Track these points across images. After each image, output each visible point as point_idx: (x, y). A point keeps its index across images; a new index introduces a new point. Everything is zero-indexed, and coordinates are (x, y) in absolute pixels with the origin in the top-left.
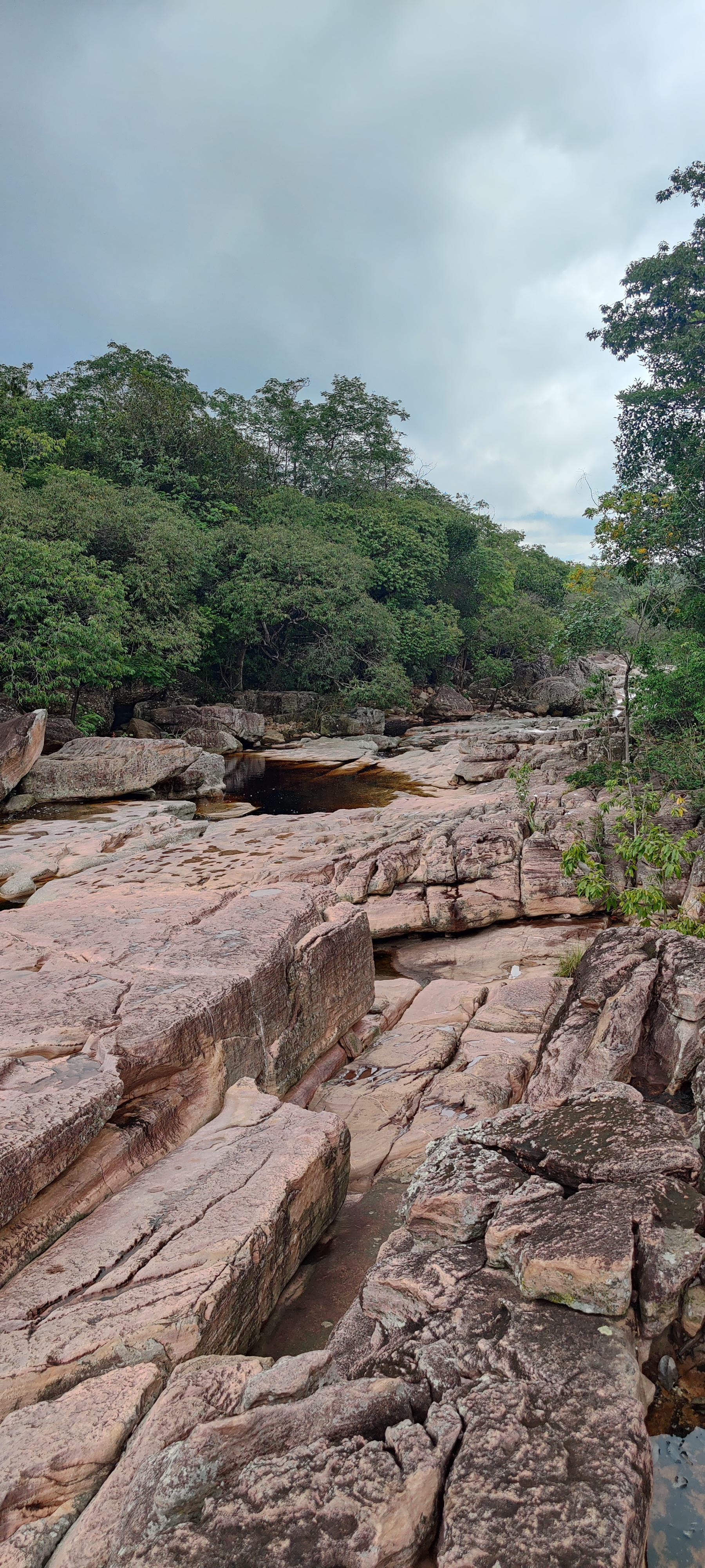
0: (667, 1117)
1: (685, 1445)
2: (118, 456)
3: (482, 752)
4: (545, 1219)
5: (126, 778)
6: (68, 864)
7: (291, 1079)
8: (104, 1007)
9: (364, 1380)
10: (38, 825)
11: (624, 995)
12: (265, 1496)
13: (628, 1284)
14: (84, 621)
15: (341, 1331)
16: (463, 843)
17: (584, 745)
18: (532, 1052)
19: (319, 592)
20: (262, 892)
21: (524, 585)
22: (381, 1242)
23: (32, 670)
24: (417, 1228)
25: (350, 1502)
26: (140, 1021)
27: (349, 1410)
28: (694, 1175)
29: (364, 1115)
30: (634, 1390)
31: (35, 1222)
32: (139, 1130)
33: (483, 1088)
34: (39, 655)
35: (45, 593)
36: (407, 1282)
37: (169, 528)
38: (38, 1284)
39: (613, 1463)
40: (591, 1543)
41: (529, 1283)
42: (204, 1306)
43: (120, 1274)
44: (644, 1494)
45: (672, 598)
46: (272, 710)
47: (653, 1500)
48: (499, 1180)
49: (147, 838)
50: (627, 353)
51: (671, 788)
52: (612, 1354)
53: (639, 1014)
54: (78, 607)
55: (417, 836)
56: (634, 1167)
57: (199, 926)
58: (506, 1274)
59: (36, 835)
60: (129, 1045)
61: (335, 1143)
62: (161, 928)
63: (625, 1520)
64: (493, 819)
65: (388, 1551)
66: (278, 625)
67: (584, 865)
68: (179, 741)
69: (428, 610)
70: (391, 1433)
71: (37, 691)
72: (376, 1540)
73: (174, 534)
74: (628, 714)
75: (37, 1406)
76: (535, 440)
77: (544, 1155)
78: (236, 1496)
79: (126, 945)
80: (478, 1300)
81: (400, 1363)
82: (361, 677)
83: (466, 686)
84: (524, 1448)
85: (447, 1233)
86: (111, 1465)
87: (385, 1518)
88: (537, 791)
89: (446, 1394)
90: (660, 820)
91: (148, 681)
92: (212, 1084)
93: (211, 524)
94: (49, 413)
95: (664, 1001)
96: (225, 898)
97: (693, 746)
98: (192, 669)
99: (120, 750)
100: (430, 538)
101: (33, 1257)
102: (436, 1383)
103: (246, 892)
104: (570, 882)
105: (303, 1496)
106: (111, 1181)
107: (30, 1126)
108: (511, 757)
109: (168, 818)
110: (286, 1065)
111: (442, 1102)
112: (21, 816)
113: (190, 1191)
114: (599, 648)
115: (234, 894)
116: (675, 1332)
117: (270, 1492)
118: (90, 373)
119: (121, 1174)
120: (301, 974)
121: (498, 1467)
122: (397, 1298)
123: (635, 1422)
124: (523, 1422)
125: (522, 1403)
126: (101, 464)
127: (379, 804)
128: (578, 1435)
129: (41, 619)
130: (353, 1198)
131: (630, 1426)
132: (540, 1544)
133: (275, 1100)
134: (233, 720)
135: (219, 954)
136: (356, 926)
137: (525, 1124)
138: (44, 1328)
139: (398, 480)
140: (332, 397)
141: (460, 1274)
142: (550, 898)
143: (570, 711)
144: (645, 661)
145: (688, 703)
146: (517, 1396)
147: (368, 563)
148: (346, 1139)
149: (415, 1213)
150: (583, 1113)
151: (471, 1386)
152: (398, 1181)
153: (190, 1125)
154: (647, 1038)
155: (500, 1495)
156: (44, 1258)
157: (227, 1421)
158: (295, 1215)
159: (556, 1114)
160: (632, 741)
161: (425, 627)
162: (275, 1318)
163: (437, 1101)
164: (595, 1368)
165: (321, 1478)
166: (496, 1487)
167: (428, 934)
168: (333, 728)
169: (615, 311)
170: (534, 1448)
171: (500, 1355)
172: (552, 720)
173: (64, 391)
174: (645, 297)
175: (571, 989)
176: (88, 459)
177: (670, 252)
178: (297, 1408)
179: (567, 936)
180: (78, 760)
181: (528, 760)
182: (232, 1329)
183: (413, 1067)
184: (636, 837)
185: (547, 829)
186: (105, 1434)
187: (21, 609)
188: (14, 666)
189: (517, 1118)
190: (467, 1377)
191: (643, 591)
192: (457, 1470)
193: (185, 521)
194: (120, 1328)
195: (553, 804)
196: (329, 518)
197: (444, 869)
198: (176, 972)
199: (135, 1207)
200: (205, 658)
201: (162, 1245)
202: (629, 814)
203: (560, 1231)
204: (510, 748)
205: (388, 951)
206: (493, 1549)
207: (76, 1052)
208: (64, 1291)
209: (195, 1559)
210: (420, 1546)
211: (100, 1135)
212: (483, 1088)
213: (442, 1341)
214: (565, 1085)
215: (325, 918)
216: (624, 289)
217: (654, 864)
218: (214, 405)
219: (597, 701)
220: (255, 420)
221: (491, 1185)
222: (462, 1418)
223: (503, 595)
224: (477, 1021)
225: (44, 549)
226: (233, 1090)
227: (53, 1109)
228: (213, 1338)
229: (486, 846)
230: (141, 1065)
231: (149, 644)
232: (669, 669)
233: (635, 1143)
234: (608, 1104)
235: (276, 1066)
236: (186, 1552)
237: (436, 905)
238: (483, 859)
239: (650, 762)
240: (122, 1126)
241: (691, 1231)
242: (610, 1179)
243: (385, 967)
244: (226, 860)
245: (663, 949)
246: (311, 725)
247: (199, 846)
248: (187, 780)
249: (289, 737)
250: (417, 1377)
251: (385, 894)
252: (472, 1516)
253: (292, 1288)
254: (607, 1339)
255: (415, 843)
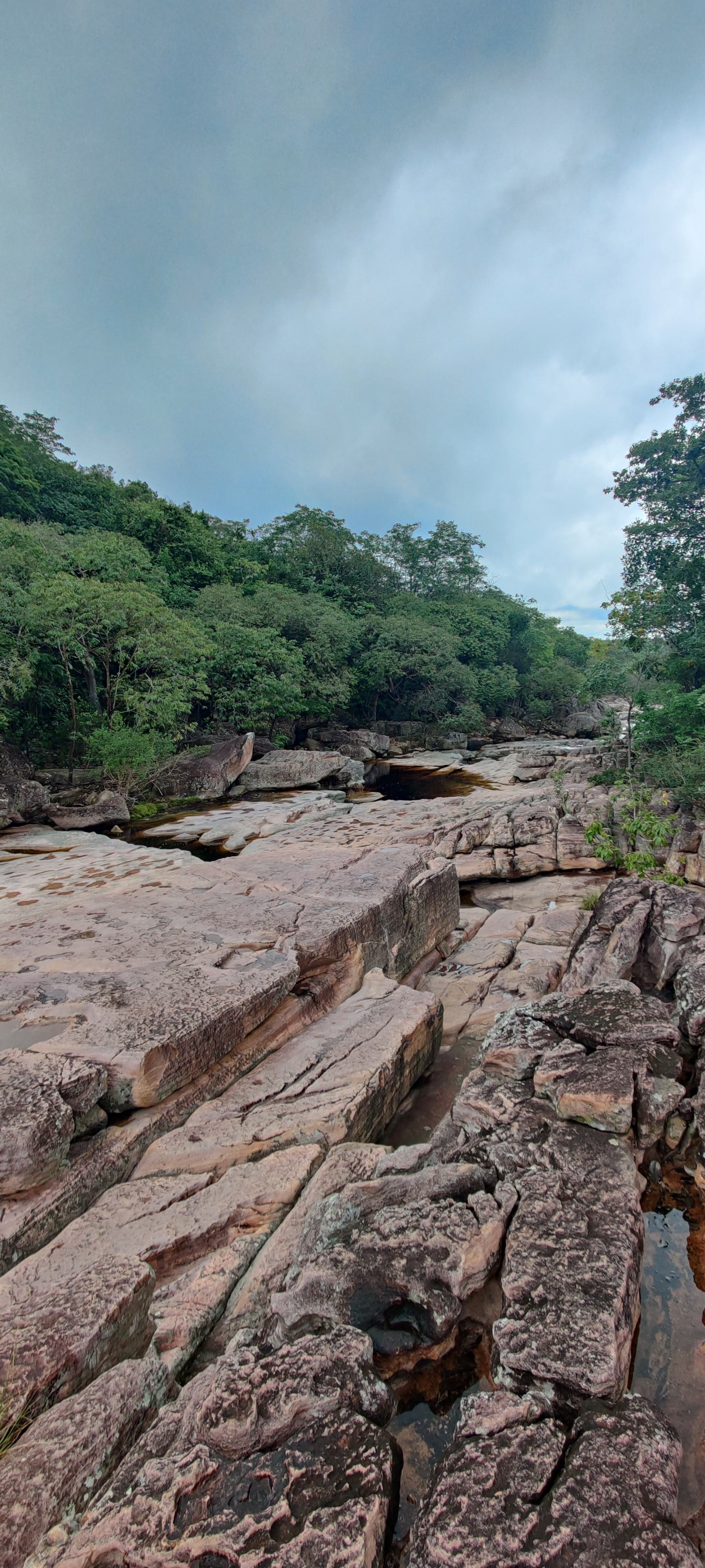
0: (656, 1004)
1: (666, 1220)
2: (301, 575)
3: (531, 761)
4: (574, 1068)
5: (302, 775)
6: (266, 829)
7: (405, 970)
8: (288, 920)
9: (454, 1164)
10: (248, 805)
11: (627, 923)
12: (390, 1231)
13: (629, 1113)
14: (278, 677)
15: (438, 1133)
16: (518, 821)
17: (600, 758)
18: (563, 959)
19: (426, 658)
20: (387, 849)
21: (560, 653)
22: (463, 1078)
23: (246, 708)
24: (488, 1070)
25: (445, 1239)
26: (310, 929)
27: (444, 1182)
28: (675, 1043)
29: (453, 995)
30: (632, 1181)
31: (245, 1052)
32: (309, 998)
33: (531, 981)
34: (251, 699)
35: (255, 660)
36: (482, 1104)
37: (331, 619)
38: (246, 1091)
39: (618, 1227)
40: (603, 1278)
41: (563, 1109)
42: (349, 1111)
43: (297, 1088)
44: (639, 1249)
45: (660, 661)
46: (395, 734)
47: (645, 1254)
48: (543, 1041)
49: (315, 814)
50: (630, 501)
51: (659, 786)
52: (618, 1157)
53: (638, 936)
54: (275, 669)
55: (489, 816)
56: (634, 1036)
57: (348, 870)
58: (547, 1102)
59: (247, 811)
60: (304, 944)
61: (433, 1012)
62: (323, 871)
63: (626, 1265)
64: (538, 804)
65: (470, 1272)
66: (399, 680)
67: (600, 837)
68: (335, 753)
69: (497, 669)
70: (471, 1198)
71: (249, 721)
72: (461, 1264)
73: (334, 622)
74: (630, 737)
75: (246, 1165)
76: (570, 560)
77: (573, 1026)
78: (372, 1230)
79: (302, 881)
80: (529, 1118)
81: (477, 1155)
82: (452, 713)
83: (521, 718)
84: (559, 1213)
85: (508, 1074)
86: (292, 1204)
87: (467, 1251)
88: (568, 787)
89: (508, 1176)
90: (652, 808)
91: (316, 715)
92: (355, 970)
93: (358, 616)
94: (259, 549)
95: (655, 927)
96: (364, 853)
97: (674, 759)
98: (345, 707)
99: (299, 758)
100: (498, 623)
101: (244, 1074)
102: (501, 1169)
103: (377, 849)
104: (590, 847)
105: (415, 1233)
106: (292, 1029)
107: (243, 992)
108: (551, 765)
109: (328, 801)
110: (402, 961)
111: (503, 989)
112: (238, 799)
113: (341, 1038)
114: (610, 694)
115: (370, 851)
116: (661, 1146)
117: (394, 1229)
118: (284, 524)
119: (298, 1025)
120: (412, 903)
121: (542, 1224)
122: (475, 1114)
123: (633, 1202)
124: (558, 1197)
125: (558, 1185)
126: (290, 580)
127: (464, 794)
128: (595, 1208)
129: (252, 677)
130: (445, 1048)
131: (629, 1205)
132: (569, 1276)
133: (395, 983)
134: (370, 740)
135: (360, 889)
136: (449, 873)
137: (560, 1005)
138: (250, 1117)
139: (477, 586)
140: (435, 534)
141: (517, 1101)
142: (577, 857)
143: (590, 735)
144: (642, 703)
145: (671, 730)
146: (554, 1180)
147: (457, 639)
148: (441, 1009)
149: (487, 1060)
150: (600, 1000)
151: (524, 1172)
152: (474, 1039)
153: (340, 996)
154: (643, 951)
155: (542, 1242)
156: (250, 1075)
157: (366, 1183)
158: (408, 1057)
159: (582, 999)
160: (633, 755)
161: (494, 680)
162: (394, 1122)
163: (501, 988)
164: (606, 1165)
165: (427, 1222)
166: (540, 1237)
167: (494, 880)
168: (434, 745)
169: (622, 475)
170: (566, 1214)
171: (543, 1153)
172: (578, 740)
173: (268, 535)
174: (642, 466)
175: (592, 918)
176: (282, 577)
177: (659, 437)
178: (411, 1178)
179: (588, 883)
180: (273, 764)
181: (562, 767)
182: (367, 1127)
183: (485, 966)
184: (636, 819)
185: (575, 812)
186: (288, 1185)
187: (240, 670)
188: (235, 705)
189: (555, 1001)
190: (521, 1166)
191: (641, 656)
192: (515, 1224)
193: (342, 614)
194: (297, 1121)
195: (578, 795)
196: (433, 611)
197: (506, 837)
198: (332, 899)
199: (306, 1046)
200: (353, 700)
201: (323, 1071)
202: (630, 803)
203: (584, 1076)
204: (550, 759)
205: (468, 890)
206: (538, 1277)
207: (270, 947)
208: (263, 1096)
209: (347, 1266)
210: (490, 1271)
211: (285, 1001)
212: (531, 981)
213: (505, 1143)
214: (587, 981)
215: (428, 867)
216: (629, 461)
217: (647, 837)
218: (360, 541)
219: (609, 728)
220: (386, 550)
221: (538, 1044)
222: (518, 1192)
223: (546, 660)
224: (527, 934)
225: (254, 633)
226: (368, 975)
227: (256, 982)
228: (355, 1131)
229: (534, 823)
230: (311, 957)
231: (318, 692)
232: (658, 707)
233: (636, 1020)
234: (617, 994)
235: (396, 961)
236: (341, 1262)
237: (501, 862)
238: (532, 831)
239: (645, 769)
240: (299, 995)
241: (672, 1080)
242: (617, 1043)
243: (467, 900)
244: (364, 829)
245: (654, 893)
246: (420, 744)
247: (347, 820)
248: (340, 777)
249: (405, 751)
250: (488, 1165)
251: (467, 853)
252: (525, 1254)
253: (405, 1104)
254: (615, 1148)
255: (486, 820)
